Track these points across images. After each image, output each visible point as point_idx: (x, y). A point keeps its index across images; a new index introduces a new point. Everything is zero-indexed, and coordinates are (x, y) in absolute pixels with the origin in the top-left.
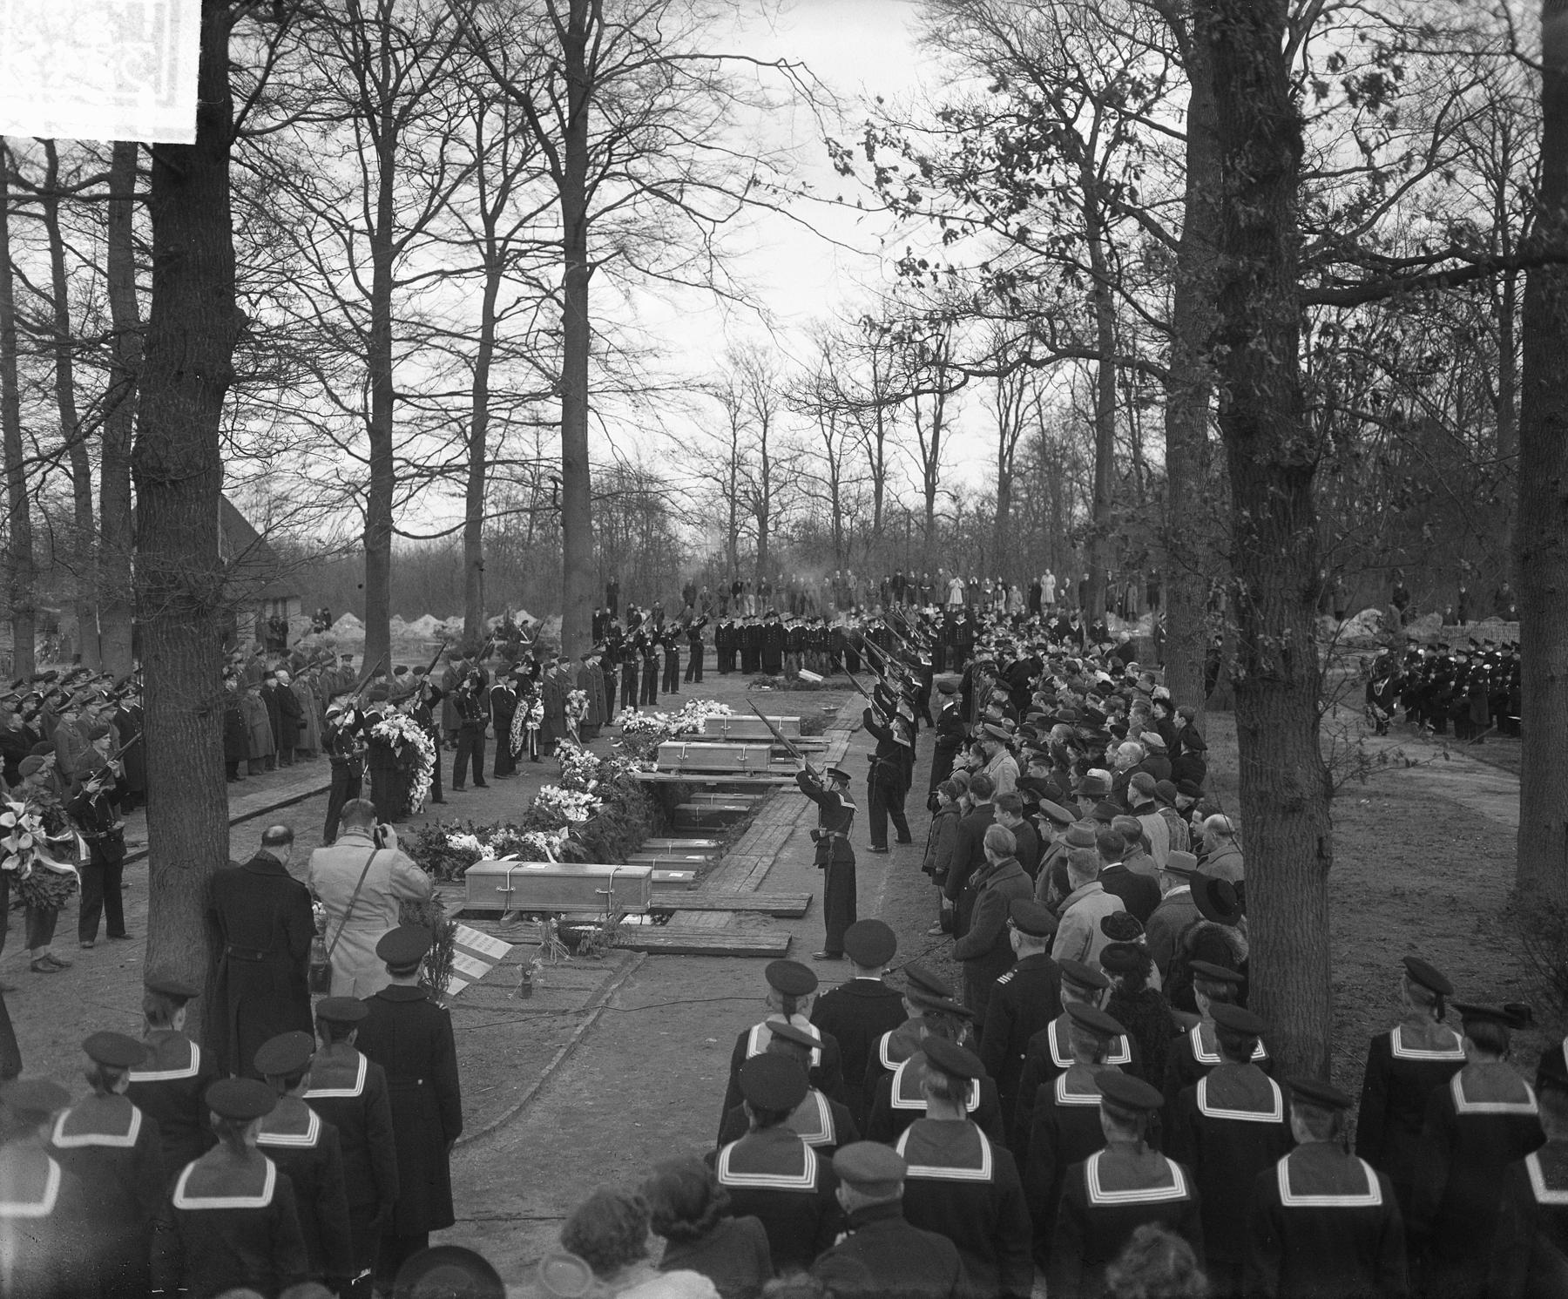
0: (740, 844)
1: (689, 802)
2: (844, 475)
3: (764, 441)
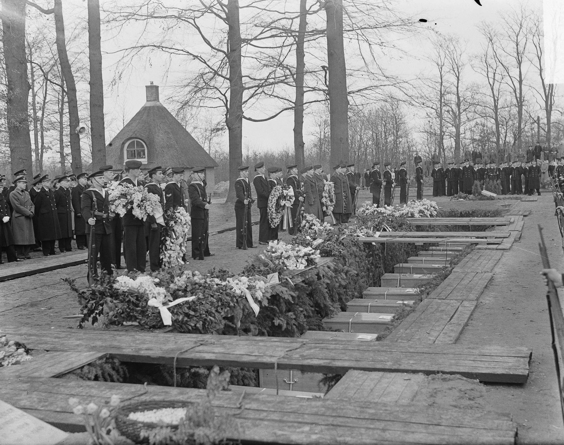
0: (439, 289)
1: (406, 262)
2: (500, 104)
3: (457, 88)
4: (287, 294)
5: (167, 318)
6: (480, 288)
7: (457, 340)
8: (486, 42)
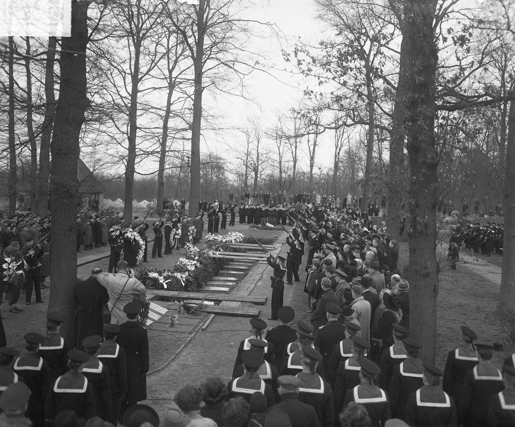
2: (283, 160)
4: (191, 279)
5: (165, 286)
6: (257, 280)
7: (249, 295)
8: (277, 120)
